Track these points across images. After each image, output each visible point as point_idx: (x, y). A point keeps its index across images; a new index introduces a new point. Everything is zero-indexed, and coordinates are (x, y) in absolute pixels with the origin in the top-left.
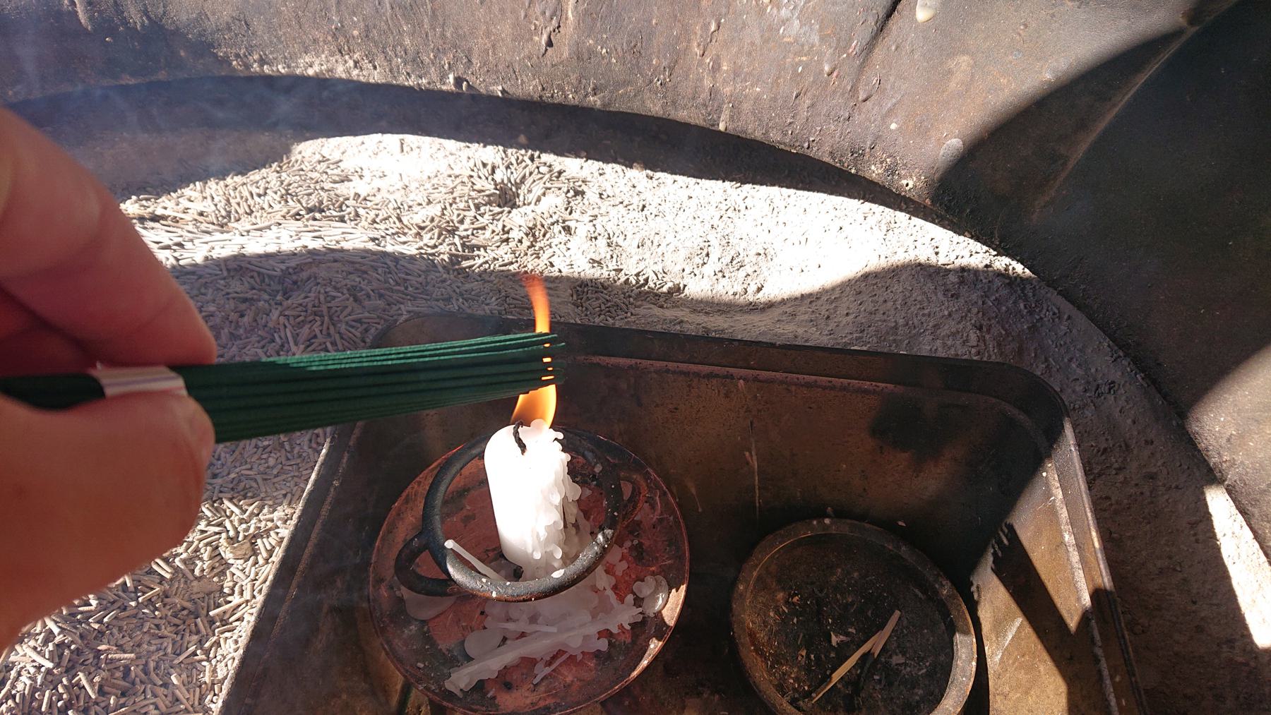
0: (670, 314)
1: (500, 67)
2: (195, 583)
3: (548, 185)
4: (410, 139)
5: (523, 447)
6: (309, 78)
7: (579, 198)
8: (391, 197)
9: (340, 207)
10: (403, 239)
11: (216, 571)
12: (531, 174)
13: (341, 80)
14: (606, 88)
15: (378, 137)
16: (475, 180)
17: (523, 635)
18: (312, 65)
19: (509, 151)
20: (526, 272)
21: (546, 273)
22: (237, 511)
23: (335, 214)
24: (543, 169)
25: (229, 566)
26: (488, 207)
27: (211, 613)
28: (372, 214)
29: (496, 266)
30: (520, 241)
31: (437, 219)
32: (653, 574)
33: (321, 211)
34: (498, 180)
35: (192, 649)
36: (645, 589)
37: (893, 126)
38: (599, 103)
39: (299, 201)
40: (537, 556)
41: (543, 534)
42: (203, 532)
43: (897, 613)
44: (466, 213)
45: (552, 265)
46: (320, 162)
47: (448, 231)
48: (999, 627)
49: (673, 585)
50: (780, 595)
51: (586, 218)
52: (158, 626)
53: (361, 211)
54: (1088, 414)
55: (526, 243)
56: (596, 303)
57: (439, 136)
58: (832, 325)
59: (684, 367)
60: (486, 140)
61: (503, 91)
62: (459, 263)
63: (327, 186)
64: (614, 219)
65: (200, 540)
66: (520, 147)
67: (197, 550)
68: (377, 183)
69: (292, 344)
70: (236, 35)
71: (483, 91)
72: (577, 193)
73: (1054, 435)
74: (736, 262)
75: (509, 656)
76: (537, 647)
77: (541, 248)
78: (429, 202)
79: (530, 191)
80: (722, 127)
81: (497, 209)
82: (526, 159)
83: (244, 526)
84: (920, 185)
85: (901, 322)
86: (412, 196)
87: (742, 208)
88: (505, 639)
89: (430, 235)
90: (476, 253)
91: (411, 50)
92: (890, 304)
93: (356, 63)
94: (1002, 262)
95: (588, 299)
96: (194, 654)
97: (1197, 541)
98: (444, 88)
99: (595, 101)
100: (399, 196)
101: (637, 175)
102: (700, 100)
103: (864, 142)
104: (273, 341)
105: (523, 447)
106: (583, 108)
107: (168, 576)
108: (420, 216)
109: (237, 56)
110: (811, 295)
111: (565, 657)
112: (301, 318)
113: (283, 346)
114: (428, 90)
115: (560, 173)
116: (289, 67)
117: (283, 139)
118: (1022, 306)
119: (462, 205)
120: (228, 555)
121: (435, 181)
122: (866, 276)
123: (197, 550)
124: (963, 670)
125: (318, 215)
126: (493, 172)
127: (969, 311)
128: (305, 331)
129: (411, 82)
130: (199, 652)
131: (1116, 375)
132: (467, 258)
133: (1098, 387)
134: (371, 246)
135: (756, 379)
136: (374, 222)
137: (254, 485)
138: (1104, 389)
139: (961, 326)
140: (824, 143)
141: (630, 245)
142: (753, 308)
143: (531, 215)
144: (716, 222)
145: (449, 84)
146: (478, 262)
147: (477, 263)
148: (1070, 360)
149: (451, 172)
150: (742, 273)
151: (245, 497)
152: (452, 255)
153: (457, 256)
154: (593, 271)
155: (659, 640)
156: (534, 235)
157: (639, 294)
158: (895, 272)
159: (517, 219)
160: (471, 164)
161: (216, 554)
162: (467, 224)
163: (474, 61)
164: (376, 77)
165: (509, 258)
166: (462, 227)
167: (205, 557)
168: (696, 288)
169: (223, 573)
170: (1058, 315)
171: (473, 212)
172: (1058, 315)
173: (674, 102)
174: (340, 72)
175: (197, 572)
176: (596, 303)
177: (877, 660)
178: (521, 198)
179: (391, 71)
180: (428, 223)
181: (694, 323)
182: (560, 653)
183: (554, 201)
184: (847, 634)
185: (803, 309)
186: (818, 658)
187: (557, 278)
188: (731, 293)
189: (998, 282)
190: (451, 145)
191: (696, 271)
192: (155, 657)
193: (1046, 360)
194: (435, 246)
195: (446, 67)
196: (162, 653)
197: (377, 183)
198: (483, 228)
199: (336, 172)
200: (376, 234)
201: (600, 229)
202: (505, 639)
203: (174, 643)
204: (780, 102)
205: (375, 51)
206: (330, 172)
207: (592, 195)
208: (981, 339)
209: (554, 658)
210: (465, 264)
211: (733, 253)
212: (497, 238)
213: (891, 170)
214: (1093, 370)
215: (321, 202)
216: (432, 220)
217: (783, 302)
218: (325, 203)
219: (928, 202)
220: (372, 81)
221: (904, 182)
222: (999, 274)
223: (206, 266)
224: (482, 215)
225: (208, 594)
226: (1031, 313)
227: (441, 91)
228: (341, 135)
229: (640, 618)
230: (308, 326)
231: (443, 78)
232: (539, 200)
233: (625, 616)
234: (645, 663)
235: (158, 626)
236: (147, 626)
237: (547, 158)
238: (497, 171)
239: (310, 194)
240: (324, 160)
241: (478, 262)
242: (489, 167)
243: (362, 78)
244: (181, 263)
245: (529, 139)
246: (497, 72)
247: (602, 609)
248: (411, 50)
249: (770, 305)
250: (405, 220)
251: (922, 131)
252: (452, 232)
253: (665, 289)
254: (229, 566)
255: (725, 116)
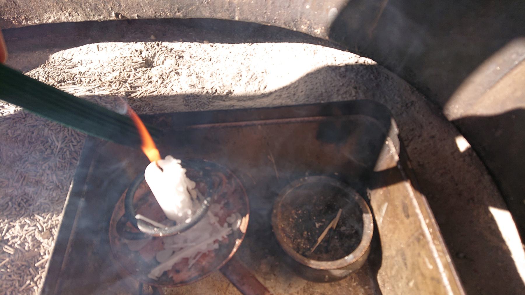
0: (228, 103)
1: (134, 6)
2: (26, 253)
3: (166, 55)
4: (101, 45)
5: (162, 169)
6: (50, 24)
7: (181, 59)
8: (96, 71)
9: (73, 78)
10: (103, 88)
11: (35, 246)
12: (158, 52)
13: (64, 23)
14: (183, 8)
15: (87, 46)
16: (133, 58)
17: (182, 249)
18: (50, 18)
19: (147, 43)
20: (161, 95)
21: (170, 94)
22: (41, 218)
23: (70, 82)
24: (163, 49)
25: (41, 243)
26: (140, 69)
27: (36, 265)
28: (88, 80)
29: (147, 94)
30: (157, 81)
31: (117, 78)
32: (234, 213)
33: (64, 82)
34: (144, 57)
35: (28, 282)
36: (231, 220)
37: (308, 7)
38: (181, 16)
39: (54, 79)
40: (180, 215)
41: (180, 206)
42: (26, 230)
43: (340, 210)
44: (131, 73)
45: (173, 90)
46: (62, 61)
47: (124, 82)
48: (380, 207)
49: (244, 215)
50: (293, 212)
51: (186, 67)
52: (10, 276)
53: (83, 79)
54: (404, 116)
55: (160, 81)
56: (195, 104)
57: (115, 41)
58: (296, 97)
59: (234, 124)
60: (136, 40)
61: (138, 16)
62: (130, 95)
63: (66, 70)
64: (198, 67)
65: (26, 234)
66: (152, 41)
67: (25, 238)
68: (89, 66)
69: (56, 142)
70: (11, 8)
71: (129, 17)
72: (180, 57)
73: (388, 127)
74: (254, 77)
75: (176, 259)
76: (188, 253)
77: (167, 83)
78: (113, 71)
79: (159, 59)
80: (237, 19)
81: (145, 69)
82: (155, 45)
83: (46, 224)
84: (323, 31)
85: (324, 91)
86: (105, 69)
87: (254, 54)
88: (174, 252)
89: (115, 84)
90: (138, 89)
91: (93, 4)
92: (318, 84)
93: (70, 14)
94: (363, 60)
95: (191, 102)
96: (30, 284)
97: (455, 160)
98: (111, 19)
99: (179, 15)
100: (99, 70)
101: (206, 46)
102: (225, 8)
103: (297, 16)
104: (48, 142)
105: (162, 169)
106: (175, 19)
107: (12, 253)
108: (110, 77)
109: (14, 18)
110: (286, 87)
111: (201, 254)
112: (59, 130)
113: (52, 143)
114: (104, 21)
115: (171, 50)
116: (40, 20)
117: (45, 54)
118: (372, 77)
119: (128, 70)
120: (39, 237)
121: (115, 61)
122: (308, 75)
123: (25, 238)
124: (368, 228)
125: (63, 84)
126: (141, 53)
127: (351, 82)
128: (61, 135)
129: (96, 19)
130: (32, 283)
131: (414, 98)
132: (133, 92)
133: (407, 104)
134: (88, 93)
135: (265, 124)
136: (89, 83)
137: (48, 206)
138: (409, 105)
139: (348, 88)
140: (279, 18)
141: (206, 77)
142: (264, 96)
143: (161, 69)
144: (243, 61)
145: (113, 17)
146: (139, 93)
147: (138, 94)
148: (394, 95)
149: (121, 56)
150: (257, 81)
151: (44, 212)
152: (126, 92)
153: (129, 92)
154: (191, 90)
155: (240, 239)
156: (163, 78)
157: (214, 97)
158: (319, 71)
159: (154, 72)
160: (130, 51)
161: (34, 239)
162: (132, 77)
163: (122, 4)
164: (80, 18)
165: (153, 89)
166: (129, 79)
167: (29, 240)
168: (239, 91)
169: (39, 246)
170: (387, 78)
171: (134, 71)
172: (387, 78)
173: (214, 11)
174: (63, 19)
175: (27, 248)
176: (195, 104)
177: (335, 230)
178: (155, 63)
179: (86, 15)
180: (114, 79)
181: (239, 105)
182: (199, 253)
183: (170, 62)
184: (322, 222)
185: (284, 93)
186: (311, 234)
187: (175, 95)
188: (253, 91)
189: (361, 68)
190: (121, 44)
191: (237, 83)
192: (10, 290)
193: (385, 97)
194: (118, 89)
195: (110, 9)
196: (13, 288)
197: (89, 66)
198: (139, 78)
199: (70, 64)
200: (90, 88)
201: (192, 71)
202: (174, 252)
203: (19, 281)
204: (259, 3)
205: (77, 7)
206: (67, 64)
207: (186, 56)
208: (357, 92)
209: (196, 256)
210: (133, 95)
211: (251, 74)
212: (146, 82)
213: (310, 27)
214: (404, 98)
215: (64, 78)
216: (116, 78)
217: (276, 91)
218: (66, 78)
219: (327, 38)
220: (78, 21)
221: (316, 31)
222: (361, 65)
223: (15, 114)
224: (138, 73)
225: (34, 257)
226: (376, 79)
227: (110, 21)
228: (71, 48)
229: (231, 232)
230: (62, 133)
231: (110, 14)
232: (163, 62)
233: (225, 232)
234: (235, 250)
235: (10, 276)
236: (4, 277)
237: (165, 44)
238: (143, 53)
239: (59, 75)
240: (64, 60)
241: (139, 93)
242: (139, 52)
243: (74, 20)
244: (4, 115)
245: (156, 37)
246: (133, 8)
247: (215, 231)
248: (93, 4)
249: (271, 93)
250: (102, 80)
251: (320, 8)
252: (125, 82)
253: (225, 93)
254: (41, 243)
255: (237, 13)
